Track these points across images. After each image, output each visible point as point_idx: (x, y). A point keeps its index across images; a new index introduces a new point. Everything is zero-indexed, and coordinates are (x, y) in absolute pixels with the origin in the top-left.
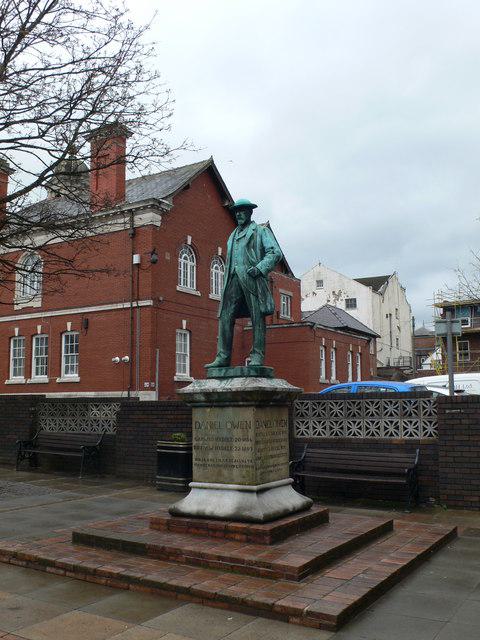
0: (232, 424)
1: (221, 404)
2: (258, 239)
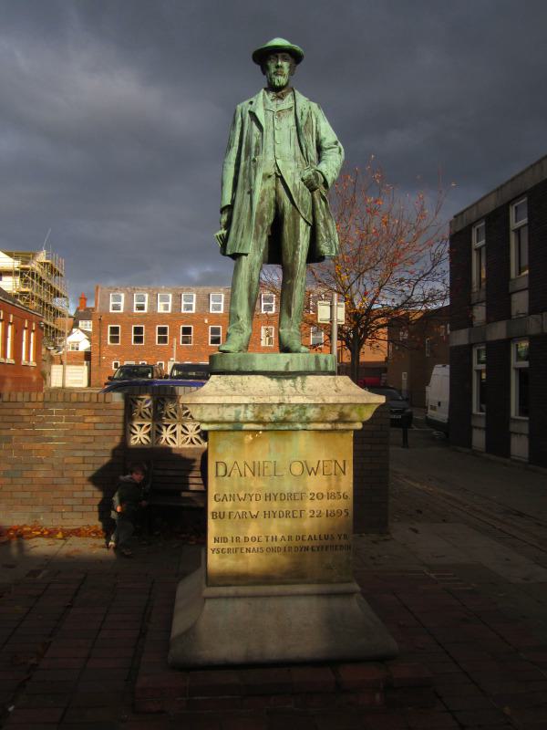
0: (305, 465)
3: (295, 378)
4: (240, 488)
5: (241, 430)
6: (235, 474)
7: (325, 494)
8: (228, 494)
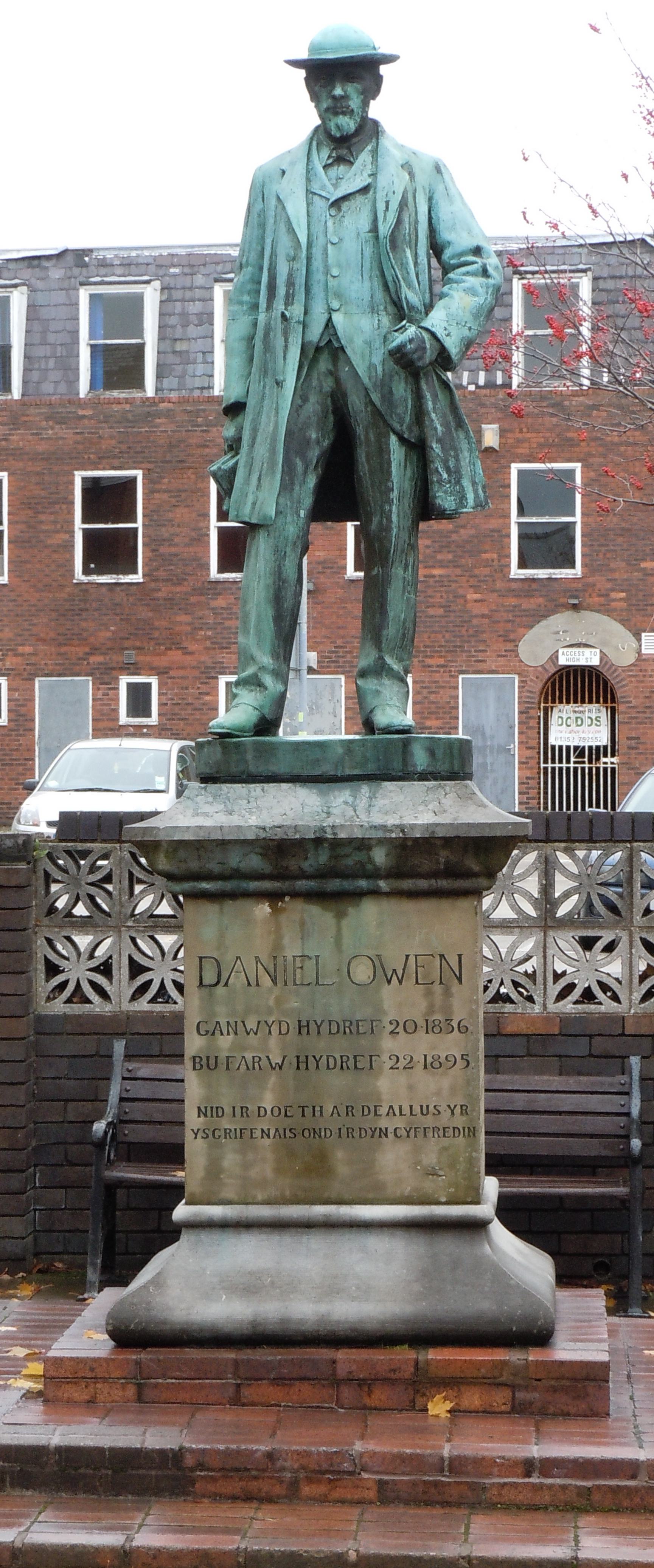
0: (378, 963)
1: (334, 884)
2: (423, 209)
3: (358, 790)
4: (248, 1011)
5: (631, 948)
6: (237, 981)
7: (421, 1022)
8: (223, 1022)
